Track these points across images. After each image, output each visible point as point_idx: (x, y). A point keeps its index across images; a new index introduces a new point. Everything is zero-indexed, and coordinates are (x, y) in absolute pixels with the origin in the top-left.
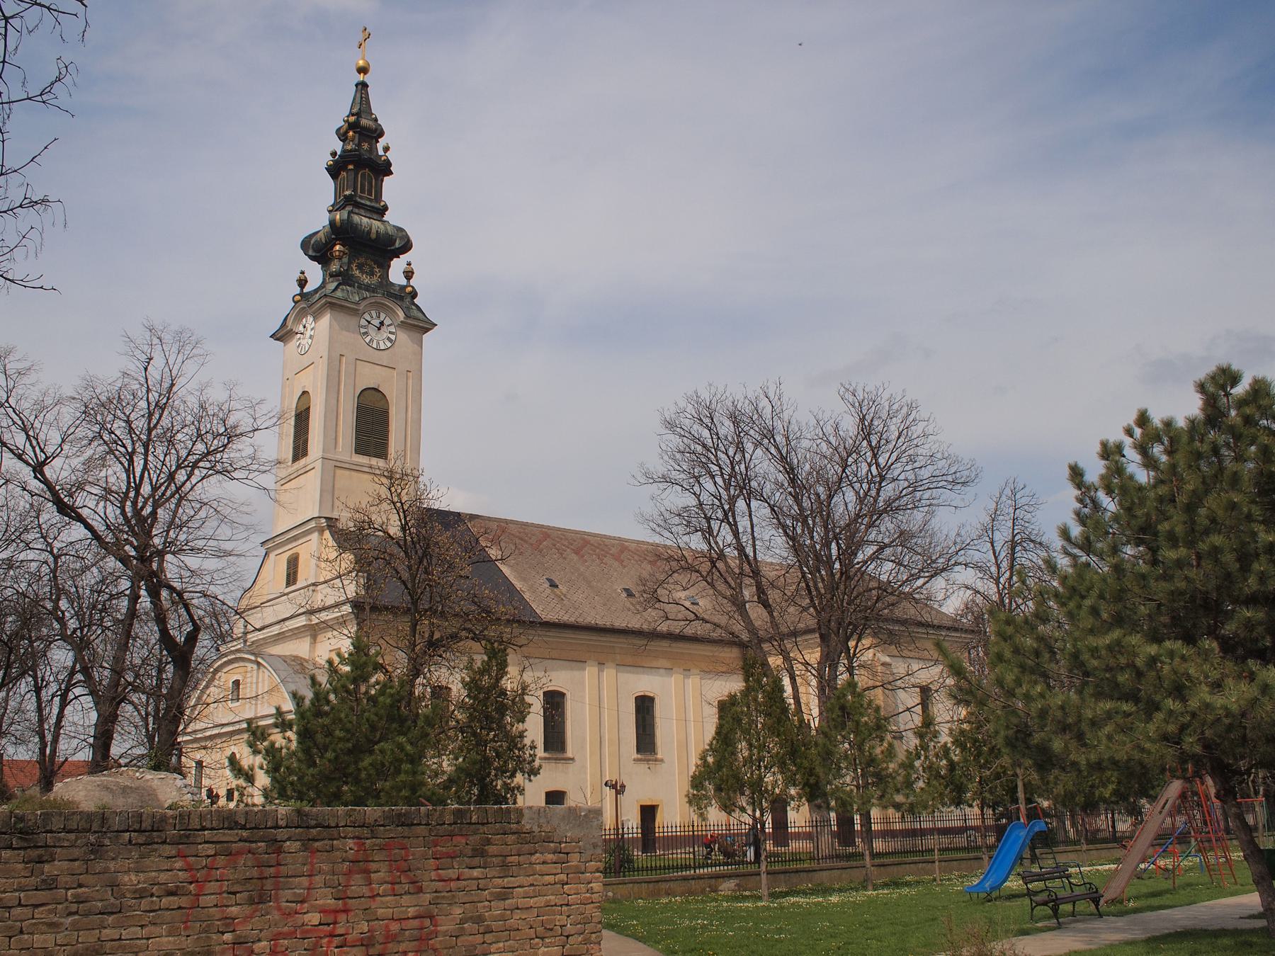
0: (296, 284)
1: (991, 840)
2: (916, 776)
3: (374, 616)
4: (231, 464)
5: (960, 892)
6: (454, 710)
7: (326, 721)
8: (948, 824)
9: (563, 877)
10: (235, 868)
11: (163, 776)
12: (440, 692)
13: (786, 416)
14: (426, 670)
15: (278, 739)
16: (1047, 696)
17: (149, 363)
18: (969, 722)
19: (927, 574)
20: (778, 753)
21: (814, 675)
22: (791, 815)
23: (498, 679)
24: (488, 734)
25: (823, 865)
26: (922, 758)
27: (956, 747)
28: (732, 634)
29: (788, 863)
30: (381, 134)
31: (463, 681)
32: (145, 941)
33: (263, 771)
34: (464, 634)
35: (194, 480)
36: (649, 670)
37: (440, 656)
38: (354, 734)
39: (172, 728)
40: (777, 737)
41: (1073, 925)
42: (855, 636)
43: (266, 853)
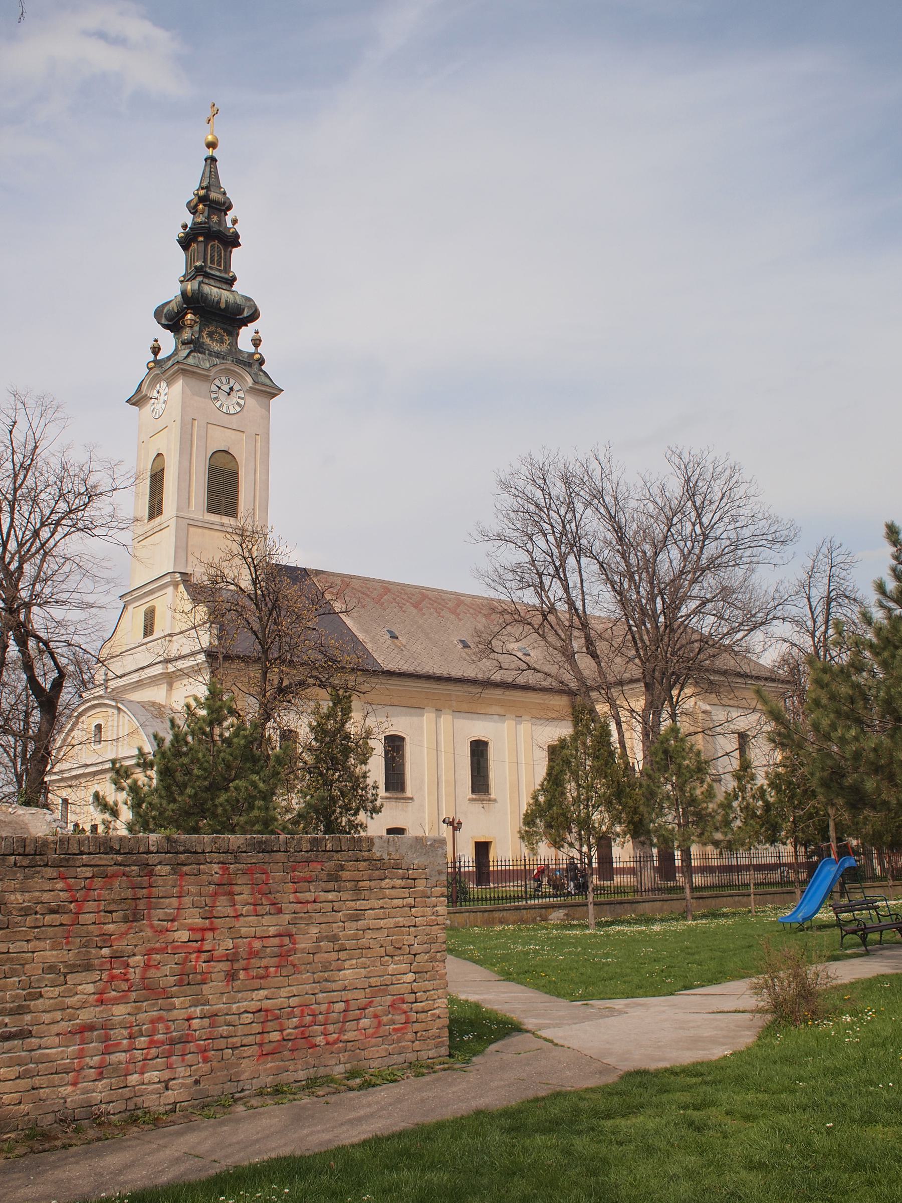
0: (150, 351)
1: (803, 876)
2: (734, 816)
3: (227, 665)
4: (92, 523)
5: (774, 922)
6: (302, 752)
7: (185, 760)
8: (762, 861)
9: (410, 900)
10: (111, 889)
11: (33, 812)
12: (288, 735)
13: (614, 477)
14: (276, 715)
15: (140, 777)
16: (861, 740)
17: (13, 426)
18: (784, 766)
19: (746, 628)
20: (605, 793)
21: (639, 722)
22: (616, 851)
23: (343, 724)
24: (333, 775)
25: (645, 896)
26: (740, 799)
27: (772, 789)
28: (562, 683)
29: (599, 896)
30: (230, 207)
31: (310, 725)
32: (30, 954)
33: (126, 807)
34: (311, 681)
35: (57, 536)
36: (483, 716)
37: (289, 702)
38: (211, 773)
39: (41, 767)
40: (605, 778)
41: (880, 952)
42: (678, 686)
43: (139, 876)
